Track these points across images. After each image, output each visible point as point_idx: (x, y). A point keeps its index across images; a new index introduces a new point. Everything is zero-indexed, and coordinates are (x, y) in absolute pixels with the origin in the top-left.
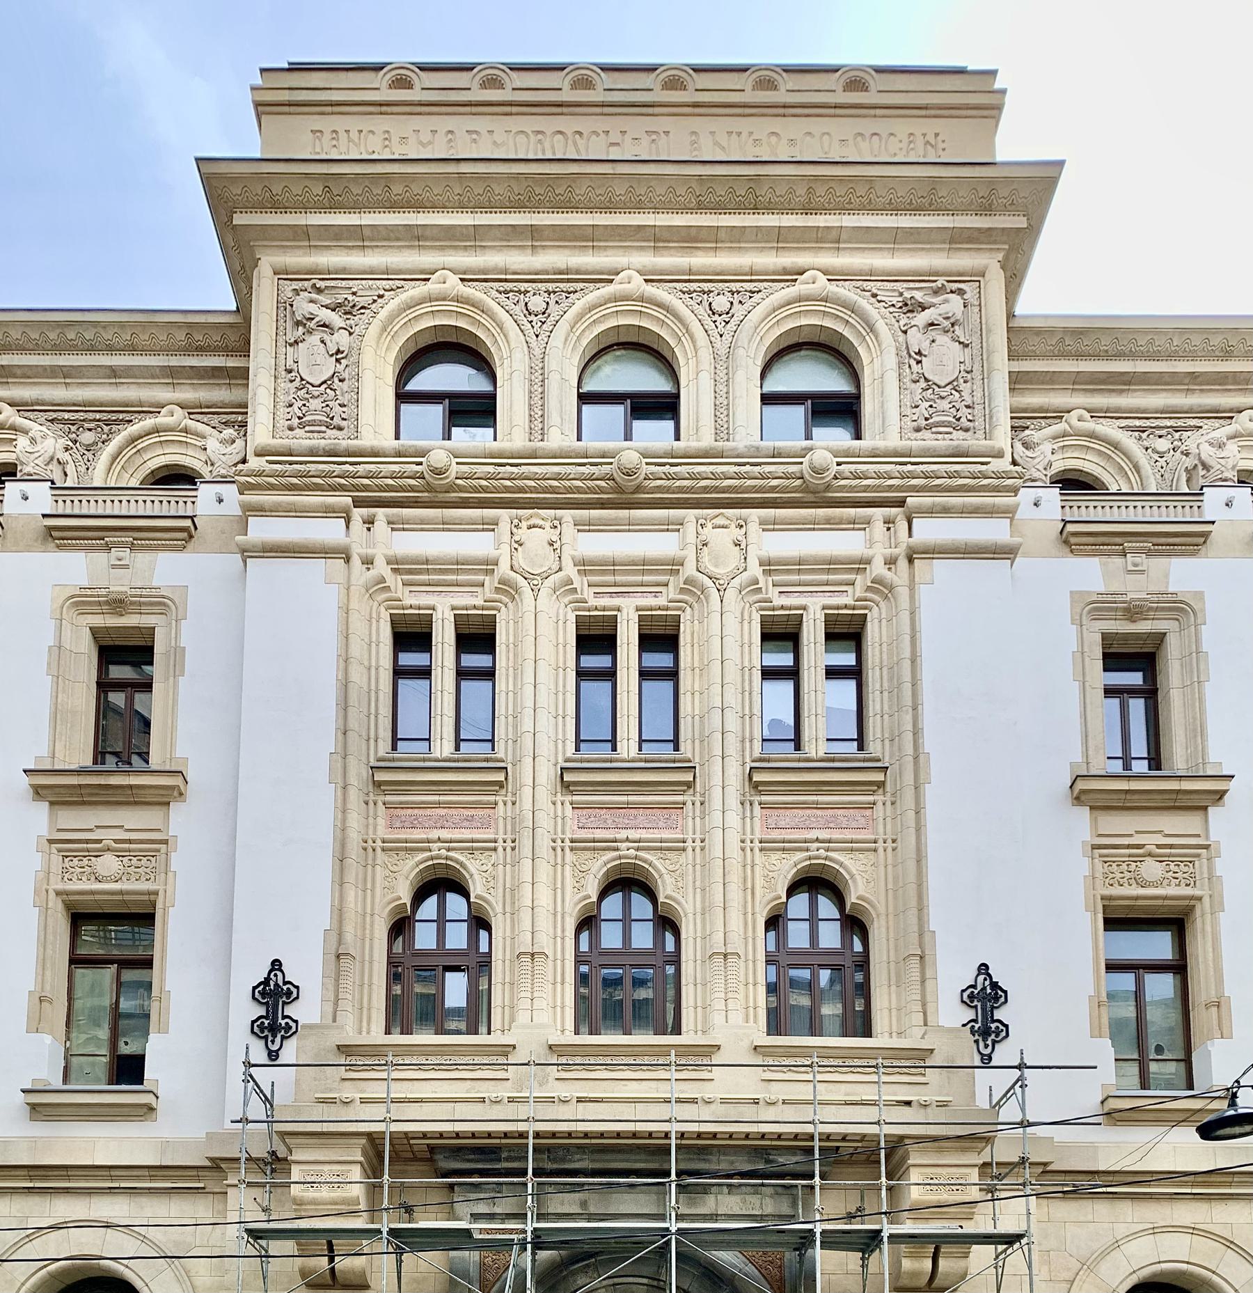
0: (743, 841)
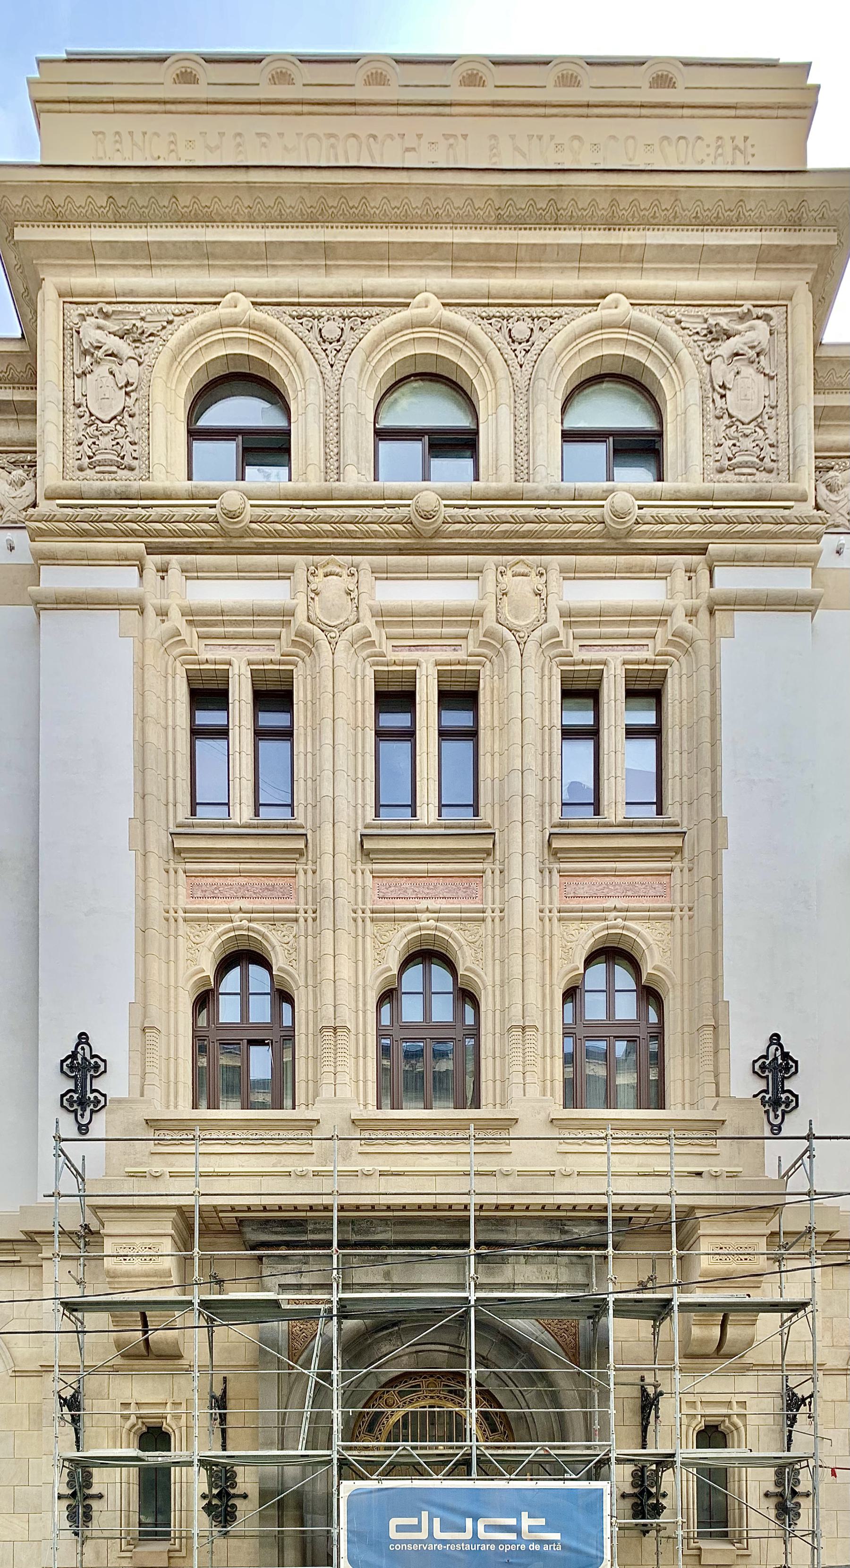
0: (541, 911)
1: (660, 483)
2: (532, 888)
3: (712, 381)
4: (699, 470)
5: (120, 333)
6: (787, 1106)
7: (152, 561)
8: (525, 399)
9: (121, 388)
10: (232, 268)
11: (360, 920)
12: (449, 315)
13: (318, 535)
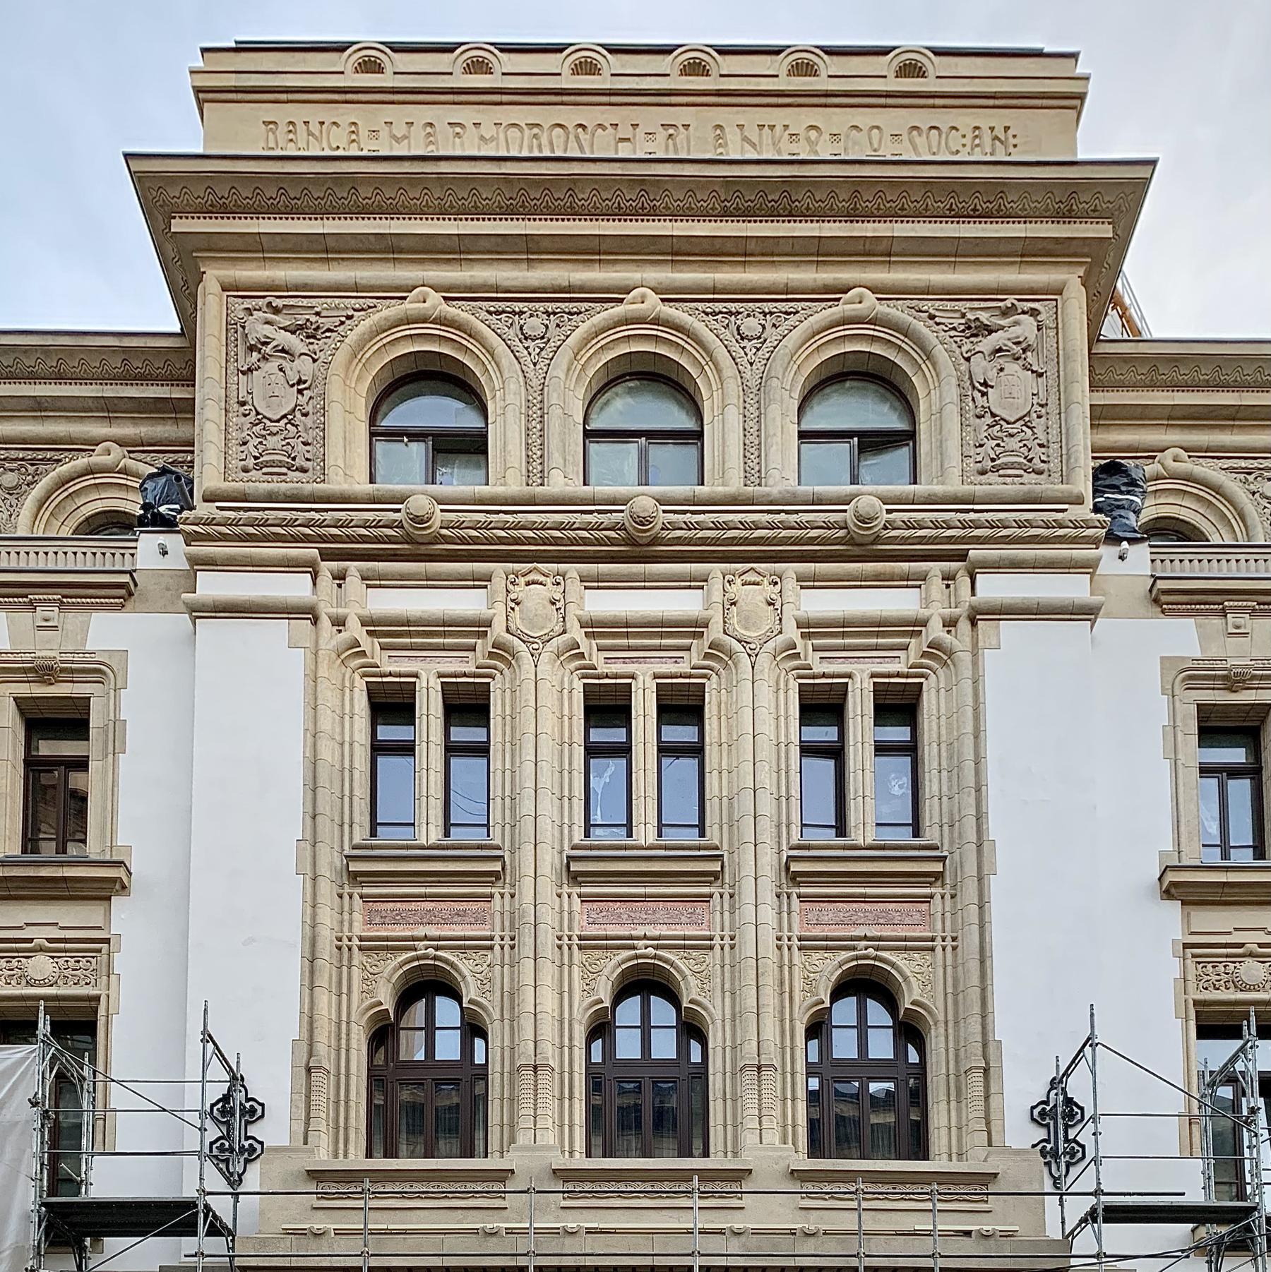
0: (779, 939)
1: (913, 487)
2: (768, 914)
3: (971, 378)
4: (957, 472)
5: (292, 328)
6: (1072, 1156)
7: (326, 567)
8: (756, 399)
9: (292, 386)
10: (421, 261)
11: (566, 948)
12: (669, 311)
13: (517, 541)
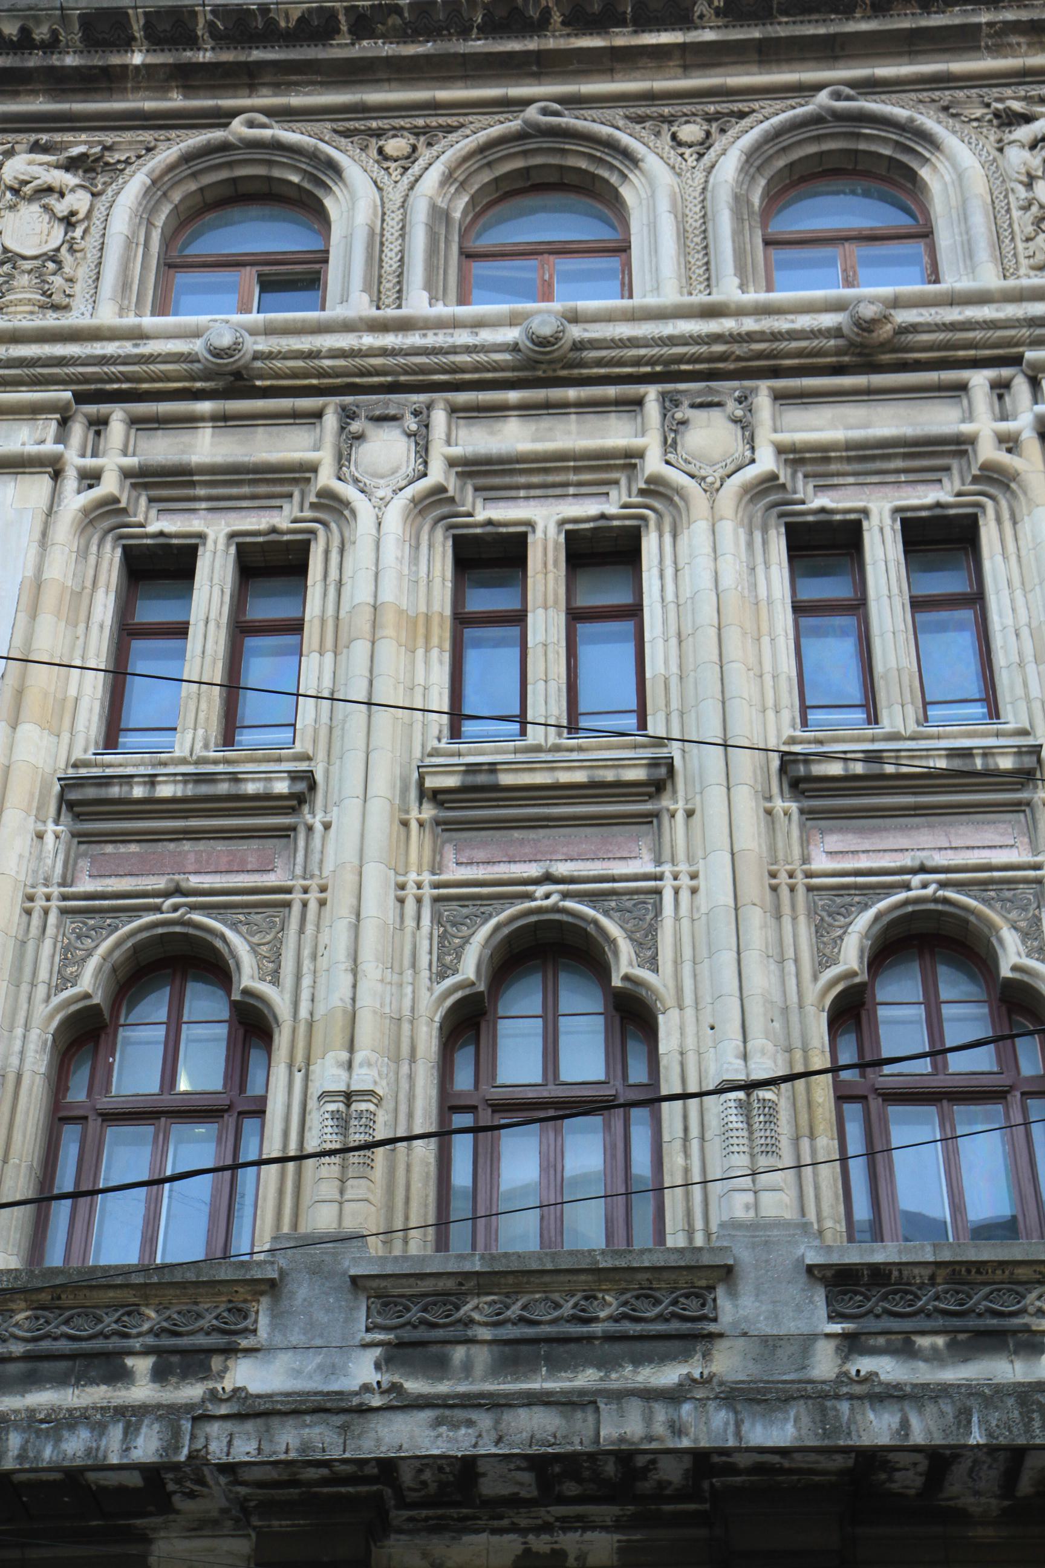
0: (773, 875)
